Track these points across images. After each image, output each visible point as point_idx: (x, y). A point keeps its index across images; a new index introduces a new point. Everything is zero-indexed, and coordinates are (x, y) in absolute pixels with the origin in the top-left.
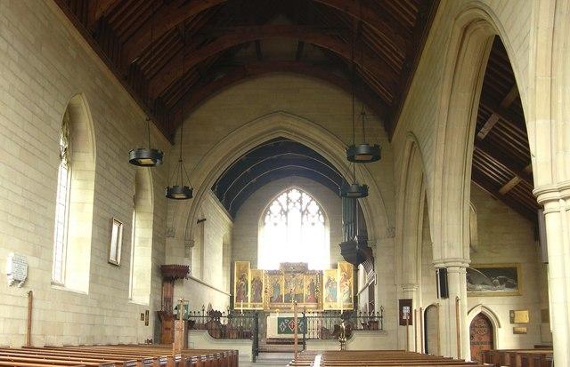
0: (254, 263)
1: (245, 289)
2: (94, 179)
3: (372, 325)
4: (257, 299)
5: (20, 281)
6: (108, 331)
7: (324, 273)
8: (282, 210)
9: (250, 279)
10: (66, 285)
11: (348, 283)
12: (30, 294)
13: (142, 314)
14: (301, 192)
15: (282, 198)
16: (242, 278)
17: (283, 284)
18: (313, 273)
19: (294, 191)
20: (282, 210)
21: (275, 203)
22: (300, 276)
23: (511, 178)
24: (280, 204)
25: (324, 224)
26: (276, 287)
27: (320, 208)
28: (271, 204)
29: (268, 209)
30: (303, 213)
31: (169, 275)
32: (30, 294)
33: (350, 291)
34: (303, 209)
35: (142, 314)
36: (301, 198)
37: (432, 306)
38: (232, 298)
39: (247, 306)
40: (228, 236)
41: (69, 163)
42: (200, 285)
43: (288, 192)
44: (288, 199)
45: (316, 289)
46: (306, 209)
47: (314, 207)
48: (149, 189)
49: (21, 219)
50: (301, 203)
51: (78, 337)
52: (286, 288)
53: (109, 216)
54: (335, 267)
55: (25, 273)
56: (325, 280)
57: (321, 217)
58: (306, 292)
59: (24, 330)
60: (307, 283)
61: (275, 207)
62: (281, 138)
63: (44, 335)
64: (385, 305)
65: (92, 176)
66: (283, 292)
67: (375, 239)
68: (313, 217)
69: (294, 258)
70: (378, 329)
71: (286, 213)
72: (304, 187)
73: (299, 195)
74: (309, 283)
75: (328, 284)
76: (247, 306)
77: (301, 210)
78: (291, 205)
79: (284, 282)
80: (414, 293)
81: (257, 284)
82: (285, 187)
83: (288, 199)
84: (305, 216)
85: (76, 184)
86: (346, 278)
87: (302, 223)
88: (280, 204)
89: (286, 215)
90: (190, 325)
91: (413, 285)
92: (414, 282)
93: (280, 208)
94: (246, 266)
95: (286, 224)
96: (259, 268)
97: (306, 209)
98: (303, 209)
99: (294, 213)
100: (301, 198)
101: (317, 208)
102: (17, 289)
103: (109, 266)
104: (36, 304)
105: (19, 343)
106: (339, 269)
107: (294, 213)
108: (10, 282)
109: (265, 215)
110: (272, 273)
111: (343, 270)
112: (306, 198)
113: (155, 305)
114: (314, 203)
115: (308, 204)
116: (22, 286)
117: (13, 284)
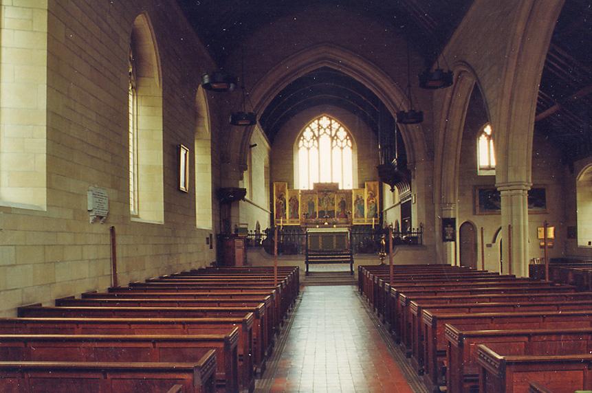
0: (290, 183)
1: (284, 207)
2: (161, 105)
3: (413, 242)
4: (294, 215)
5: (101, 217)
6: (183, 260)
7: (353, 192)
8: (314, 135)
9: (287, 197)
10: (140, 216)
11: (374, 201)
12: (112, 230)
13: (207, 238)
14: (330, 119)
15: (314, 125)
16: (281, 197)
17: (317, 202)
18: (344, 192)
19: (325, 118)
20: (314, 135)
21: (308, 129)
22: (331, 195)
23: (554, 104)
24: (312, 130)
25: (352, 148)
26: (311, 205)
27: (348, 135)
28: (304, 130)
29: (302, 135)
30: (332, 138)
31: (228, 197)
32: (112, 230)
33: (376, 207)
34: (333, 135)
35: (207, 238)
36: (330, 125)
37: (466, 222)
38: (272, 215)
39: (285, 222)
40: (268, 160)
41: (135, 88)
42: (251, 205)
43: (319, 119)
44: (319, 125)
45: (345, 205)
46: (336, 135)
47: (342, 133)
48: (206, 117)
49: (98, 148)
50: (331, 130)
51: (158, 268)
52: (319, 205)
53: (175, 142)
54: (362, 186)
55: (106, 207)
56: (354, 199)
57: (349, 142)
58: (337, 209)
59: (108, 269)
60: (337, 201)
61: (307, 133)
62: (325, 68)
63: (128, 272)
64: (424, 222)
65: (160, 102)
66: (317, 209)
67: (415, 162)
68: (308, 142)
69: (326, 179)
70: (417, 244)
71: (318, 139)
72: (333, 115)
73: (329, 122)
74: (339, 201)
75: (356, 201)
76: (285, 222)
77: (331, 136)
78: (322, 131)
79: (317, 200)
80: (452, 212)
81: (294, 200)
82: (317, 114)
83: (319, 125)
84: (334, 141)
85: (142, 110)
86: (372, 196)
87: (332, 148)
88: (312, 130)
89: (318, 141)
90: (248, 244)
91: (450, 204)
92: (452, 201)
93: (312, 134)
94: (284, 186)
95: (318, 148)
96: (295, 188)
97: (336, 135)
98: (333, 135)
99: (325, 140)
100: (330, 125)
101: (345, 134)
102: (102, 228)
103: (177, 198)
104: (119, 240)
105: (104, 286)
106: (366, 189)
107: (325, 140)
108: (91, 219)
109: (299, 139)
110: (305, 193)
111: (369, 190)
112: (335, 125)
113: (216, 231)
114: (342, 129)
115: (338, 130)
116: (104, 222)
117: (95, 221)
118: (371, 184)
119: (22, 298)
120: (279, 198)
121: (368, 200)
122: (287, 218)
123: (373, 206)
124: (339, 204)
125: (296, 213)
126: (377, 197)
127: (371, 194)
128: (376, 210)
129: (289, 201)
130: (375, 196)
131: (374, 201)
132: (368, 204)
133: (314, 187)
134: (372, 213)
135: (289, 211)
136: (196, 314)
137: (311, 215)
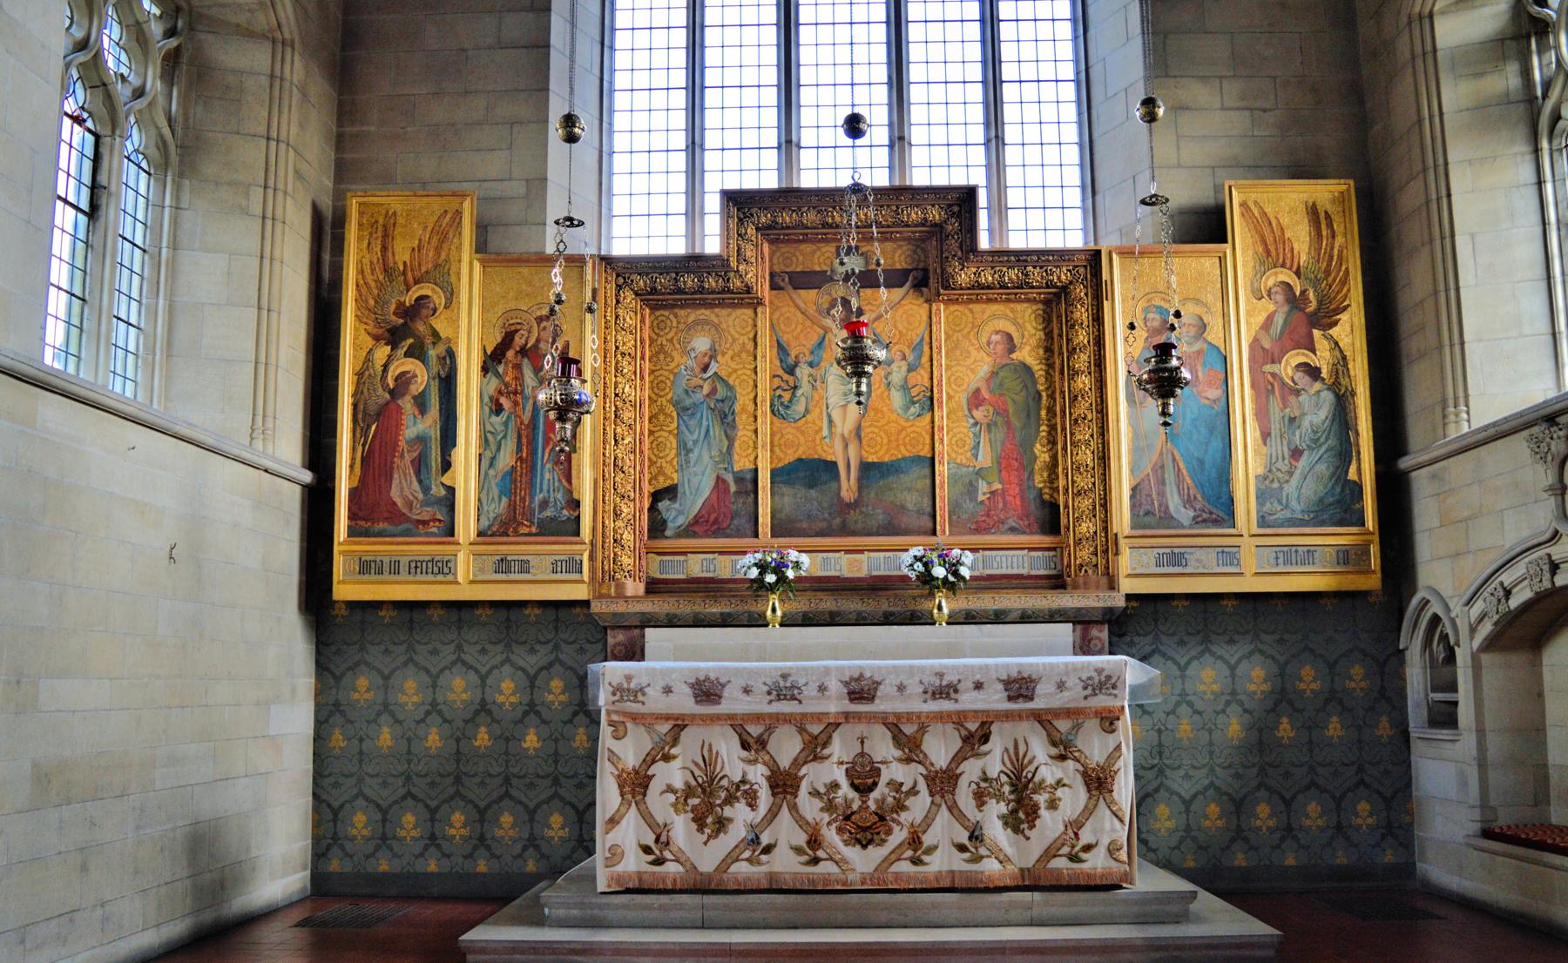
9: (468, 334)
11: (1323, 358)
16: (404, 328)
38: (317, 501)
86: (1309, 315)
94: (444, 233)
111: (1272, 252)
118: (1289, 202)
119: (234, 71)
120: (393, 337)
121: (1262, 356)
122: (467, 523)
123: (1316, 409)
124: (976, 400)
125: (548, 475)
126: (1350, 330)
127: (1294, 301)
128: (1345, 453)
129: (492, 361)
130: (1325, 317)
131: (1323, 358)
132: (1265, 387)
133: (310, 469)
134: (1306, 483)
135: (487, 460)
136: (828, 604)
137: (697, 492)
